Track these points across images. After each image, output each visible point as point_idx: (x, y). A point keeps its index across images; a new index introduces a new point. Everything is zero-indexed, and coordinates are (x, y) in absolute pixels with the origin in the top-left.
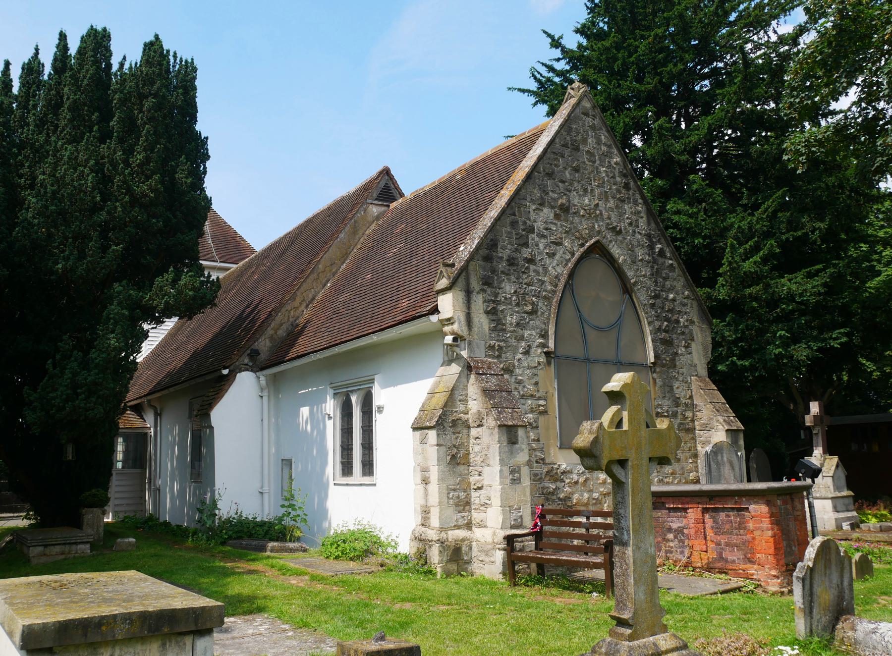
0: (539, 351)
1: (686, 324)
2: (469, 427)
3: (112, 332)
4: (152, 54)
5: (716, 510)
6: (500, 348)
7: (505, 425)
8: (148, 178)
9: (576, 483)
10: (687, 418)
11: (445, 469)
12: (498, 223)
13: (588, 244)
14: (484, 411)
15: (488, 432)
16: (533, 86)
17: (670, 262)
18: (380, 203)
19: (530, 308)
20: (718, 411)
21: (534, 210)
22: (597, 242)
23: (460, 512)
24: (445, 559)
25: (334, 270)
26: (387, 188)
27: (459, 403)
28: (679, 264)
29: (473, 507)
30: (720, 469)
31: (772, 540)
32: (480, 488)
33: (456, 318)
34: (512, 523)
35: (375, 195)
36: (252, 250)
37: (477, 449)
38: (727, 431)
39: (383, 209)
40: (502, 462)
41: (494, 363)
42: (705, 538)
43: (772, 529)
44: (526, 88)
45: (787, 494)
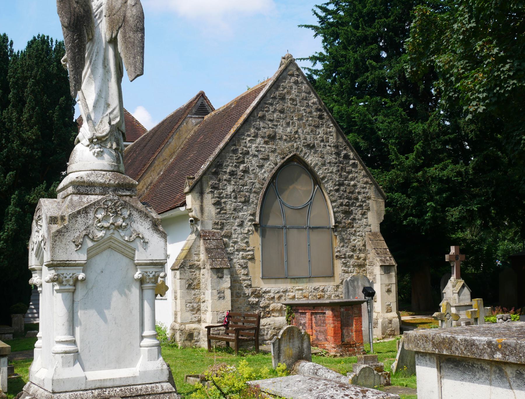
0: (250, 223)
1: (363, 200)
2: (200, 269)
3: (11, 220)
4: (32, 50)
5: (316, 313)
6: (222, 224)
7: (214, 268)
8: (32, 128)
10: (360, 258)
12: (223, 151)
13: (287, 157)
14: (206, 260)
15: (207, 271)
16: (316, 22)
17: (353, 161)
18: (197, 116)
19: (244, 199)
20: (378, 254)
21: (249, 141)
22: (295, 155)
23: (193, 314)
24: (183, 339)
25: (165, 163)
26: (202, 106)
27: (194, 255)
28: (360, 162)
29: (202, 312)
30: (355, 290)
31: (333, 329)
32: (204, 302)
33: (193, 209)
34: (218, 320)
35: (194, 111)
36: (144, 130)
37: (203, 280)
38: (381, 266)
39: (200, 120)
40: (213, 288)
41: (218, 233)
42: (312, 328)
43: (334, 323)
44: (309, 24)
45: (350, 305)
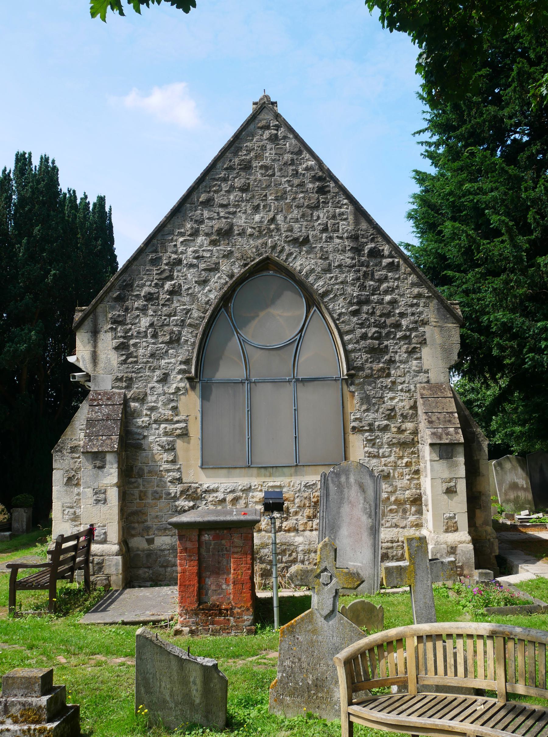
0: (180, 377)
7: (88, 452)
9: (224, 500)
11: (62, 490)
19: (168, 337)
27: (80, 432)
